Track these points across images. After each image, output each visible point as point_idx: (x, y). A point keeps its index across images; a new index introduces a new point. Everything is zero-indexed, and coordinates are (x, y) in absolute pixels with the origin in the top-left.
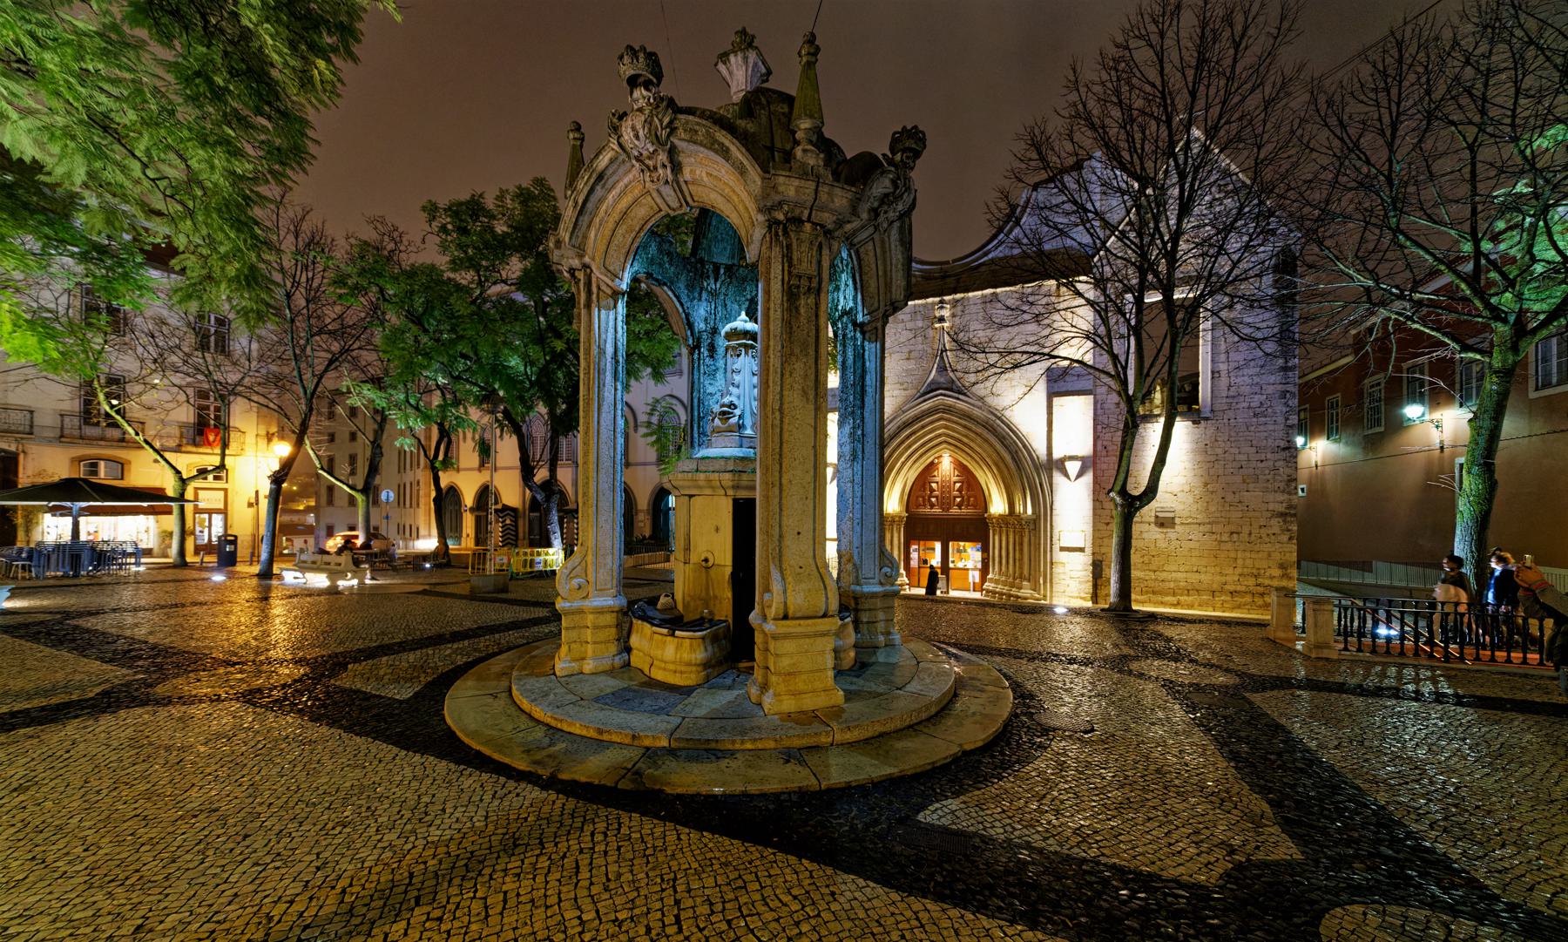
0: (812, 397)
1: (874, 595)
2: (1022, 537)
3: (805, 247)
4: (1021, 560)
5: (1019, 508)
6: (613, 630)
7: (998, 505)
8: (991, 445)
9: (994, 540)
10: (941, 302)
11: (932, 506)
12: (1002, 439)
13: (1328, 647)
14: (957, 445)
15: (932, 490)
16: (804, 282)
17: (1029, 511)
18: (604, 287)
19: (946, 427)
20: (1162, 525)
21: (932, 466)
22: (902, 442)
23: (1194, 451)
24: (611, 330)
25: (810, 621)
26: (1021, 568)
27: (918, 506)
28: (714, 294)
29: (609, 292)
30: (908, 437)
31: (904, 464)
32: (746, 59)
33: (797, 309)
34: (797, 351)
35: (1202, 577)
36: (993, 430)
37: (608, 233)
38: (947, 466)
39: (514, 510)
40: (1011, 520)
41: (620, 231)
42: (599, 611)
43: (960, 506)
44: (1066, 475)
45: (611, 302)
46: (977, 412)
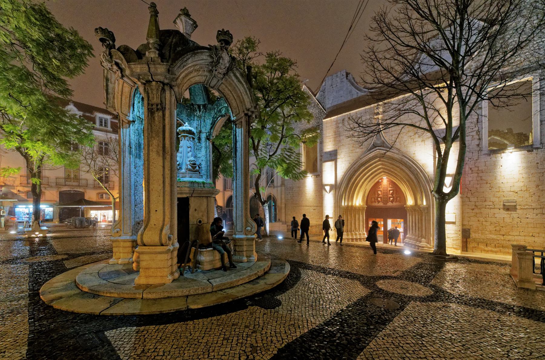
0: (161, 154)
1: (241, 239)
2: (422, 217)
3: (155, 92)
4: (422, 227)
5: (419, 202)
6: (130, 249)
7: (410, 202)
8: (404, 171)
9: (409, 218)
10: (378, 106)
11: (379, 202)
12: (409, 168)
13: (529, 281)
14: (389, 173)
15: (379, 195)
16: (154, 107)
17: (425, 203)
18: (124, 120)
19: (382, 164)
20: (508, 210)
21: (378, 184)
22: (362, 173)
23: (528, 167)
24: (128, 136)
25: (153, 247)
26: (422, 231)
27: (372, 202)
28: (200, 117)
29: (127, 122)
30: (364, 170)
31: (363, 183)
32: (181, 20)
33: (154, 119)
34: (154, 135)
35: (536, 239)
36: (405, 164)
37: (120, 99)
38: (385, 181)
39: (221, 207)
40: (416, 208)
41: (123, 98)
42: (124, 241)
43: (392, 202)
44: (446, 186)
45: (128, 125)
46: (396, 156)
